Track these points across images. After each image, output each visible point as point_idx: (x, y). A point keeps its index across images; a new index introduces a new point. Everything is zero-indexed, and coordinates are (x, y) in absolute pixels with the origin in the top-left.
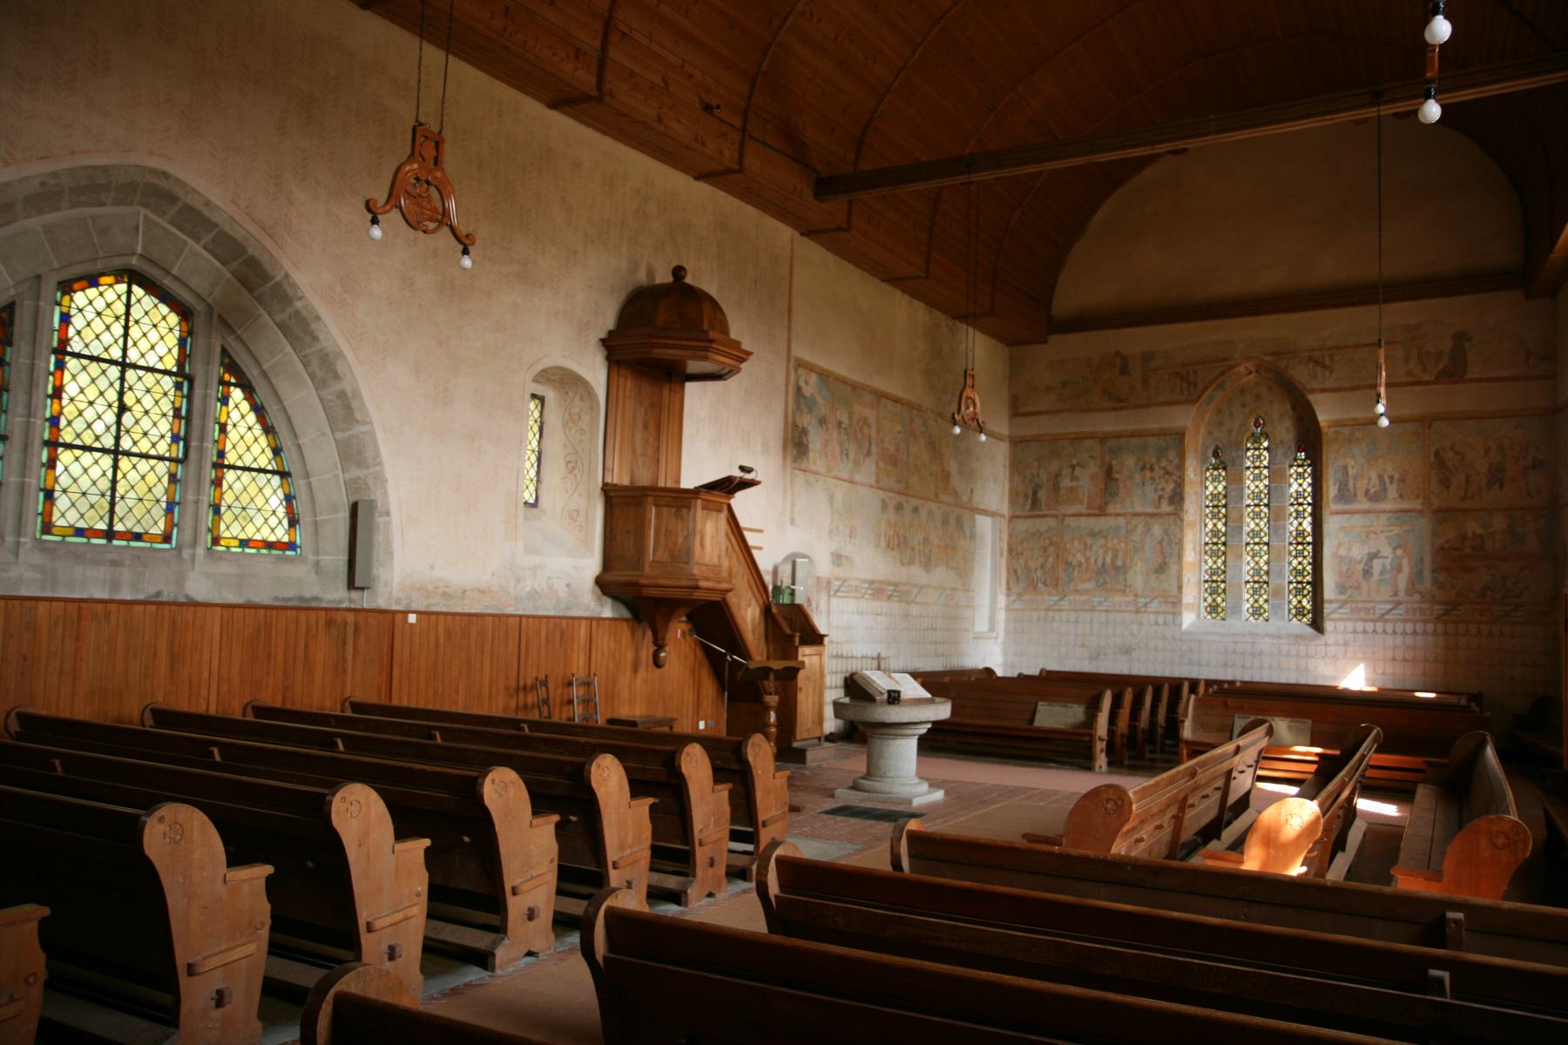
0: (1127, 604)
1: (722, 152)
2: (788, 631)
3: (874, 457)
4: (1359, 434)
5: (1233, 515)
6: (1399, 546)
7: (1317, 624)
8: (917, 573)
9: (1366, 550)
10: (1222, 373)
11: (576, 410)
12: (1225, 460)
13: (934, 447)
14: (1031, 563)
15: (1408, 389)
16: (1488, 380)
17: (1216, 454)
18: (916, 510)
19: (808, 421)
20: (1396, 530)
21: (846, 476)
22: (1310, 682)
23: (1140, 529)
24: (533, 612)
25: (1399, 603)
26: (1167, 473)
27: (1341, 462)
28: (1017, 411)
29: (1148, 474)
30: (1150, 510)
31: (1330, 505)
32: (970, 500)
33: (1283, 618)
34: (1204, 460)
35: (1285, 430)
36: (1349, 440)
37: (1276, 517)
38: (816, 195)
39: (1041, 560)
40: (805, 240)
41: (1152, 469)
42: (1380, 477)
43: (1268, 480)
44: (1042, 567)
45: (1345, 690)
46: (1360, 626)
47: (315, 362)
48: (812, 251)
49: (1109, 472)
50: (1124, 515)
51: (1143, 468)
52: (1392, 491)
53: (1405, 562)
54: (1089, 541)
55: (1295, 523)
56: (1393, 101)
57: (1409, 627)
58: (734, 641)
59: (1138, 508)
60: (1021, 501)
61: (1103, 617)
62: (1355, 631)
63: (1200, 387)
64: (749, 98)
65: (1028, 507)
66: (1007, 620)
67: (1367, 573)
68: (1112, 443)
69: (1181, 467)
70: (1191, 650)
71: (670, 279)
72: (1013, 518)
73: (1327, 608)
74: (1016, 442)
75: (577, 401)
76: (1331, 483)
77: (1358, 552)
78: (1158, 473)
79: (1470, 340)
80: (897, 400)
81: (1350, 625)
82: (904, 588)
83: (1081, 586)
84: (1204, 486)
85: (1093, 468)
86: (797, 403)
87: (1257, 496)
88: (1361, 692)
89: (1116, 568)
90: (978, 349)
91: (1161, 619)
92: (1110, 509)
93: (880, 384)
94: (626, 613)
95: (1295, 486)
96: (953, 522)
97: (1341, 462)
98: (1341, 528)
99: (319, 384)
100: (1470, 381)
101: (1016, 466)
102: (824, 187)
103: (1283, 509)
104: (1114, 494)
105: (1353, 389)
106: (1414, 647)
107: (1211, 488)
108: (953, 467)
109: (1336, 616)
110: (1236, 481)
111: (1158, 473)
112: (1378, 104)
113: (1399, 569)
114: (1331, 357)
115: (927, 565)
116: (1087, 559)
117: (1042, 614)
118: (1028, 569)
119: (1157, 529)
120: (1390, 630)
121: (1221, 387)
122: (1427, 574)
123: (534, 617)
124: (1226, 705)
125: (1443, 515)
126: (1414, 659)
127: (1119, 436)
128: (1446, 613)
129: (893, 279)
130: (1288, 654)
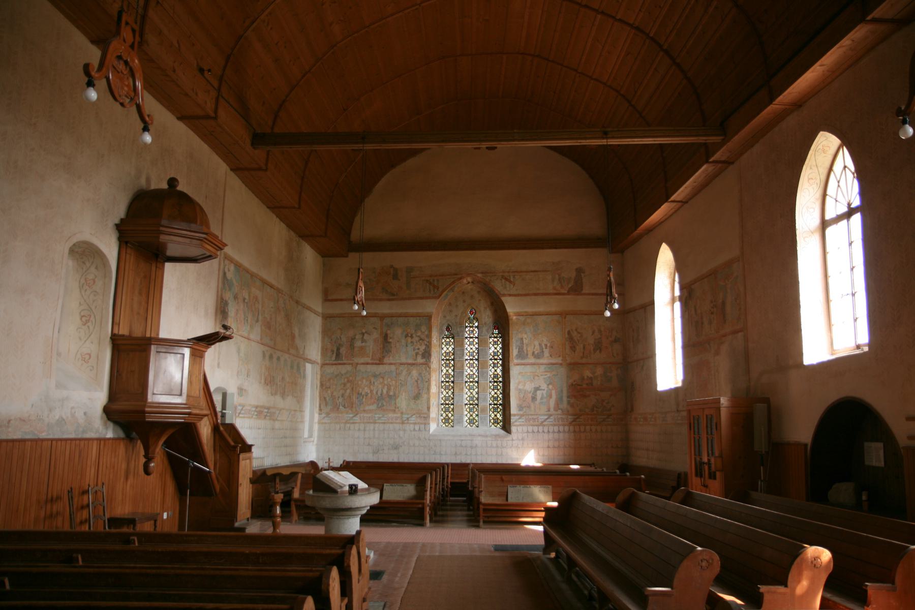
0: (397, 418)
1: (206, 102)
2: (232, 444)
4: (529, 321)
5: (458, 365)
6: (550, 384)
7: (506, 427)
8: (279, 401)
9: (533, 385)
10: (453, 282)
11: (91, 277)
12: (453, 332)
13: (288, 317)
16: (593, 294)
17: (448, 329)
18: (278, 359)
19: (228, 296)
20: (549, 374)
21: (246, 334)
22: (504, 462)
23: (404, 373)
24: (60, 437)
25: (551, 415)
28: (327, 297)
29: (409, 340)
30: (410, 361)
34: (441, 332)
35: (487, 316)
36: (524, 324)
37: (482, 366)
38: (252, 144)
39: (342, 392)
40: (232, 174)
41: (412, 337)
42: (540, 345)
43: (476, 344)
48: (235, 181)
49: (385, 337)
51: (407, 336)
52: (547, 353)
53: (553, 392)
56: (613, 138)
57: (556, 429)
58: (198, 454)
59: (404, 360)
61: (382, 427)
62: (528, 432)
63: (440, 290)
64: (224, 70)
65: (334, 358)
66: (319, 430)
67: (534, 398)
68: (387, 320)
69: (429, 336)
70: (435, 446)
71: (165, 186)
73: (513, 419)
74: (326, 317)
75: (93, 269)
77: (529, 387)
78: (416, 339)
80: (272, 286)
81: (525, 428)
82: (272, 410)
83: (367, 408)
85: (376, 335)
86: (224, 284)
87: (472, 354)
88: (534, 467)
89: (390, 397)
90: (309, 256)
91: (417, 428)
92: (386, 360)
93: (264, 275)
94: (121, 434)
96: (295, 367)
97: (520, 336)
98: (520, 373)
100: (585, 294)
103: (487, 362)
107: (445, 349)
108: (296, 331)
111: (416, 339)
112: (607, 138)
113: (551, 396)
114: (514, 277)
115: (283, 395)
116: (371, 391)
117: (342, 425)
119: (415, 373)
120: (546, 430)
121: (452, 290)
122: (565, 399)
123: (61, 440)
124: (502, 480)
125: (573, 366)
126: (559, 447)
127: (391, 316)
129: (275, 207)
130: (492, 446)
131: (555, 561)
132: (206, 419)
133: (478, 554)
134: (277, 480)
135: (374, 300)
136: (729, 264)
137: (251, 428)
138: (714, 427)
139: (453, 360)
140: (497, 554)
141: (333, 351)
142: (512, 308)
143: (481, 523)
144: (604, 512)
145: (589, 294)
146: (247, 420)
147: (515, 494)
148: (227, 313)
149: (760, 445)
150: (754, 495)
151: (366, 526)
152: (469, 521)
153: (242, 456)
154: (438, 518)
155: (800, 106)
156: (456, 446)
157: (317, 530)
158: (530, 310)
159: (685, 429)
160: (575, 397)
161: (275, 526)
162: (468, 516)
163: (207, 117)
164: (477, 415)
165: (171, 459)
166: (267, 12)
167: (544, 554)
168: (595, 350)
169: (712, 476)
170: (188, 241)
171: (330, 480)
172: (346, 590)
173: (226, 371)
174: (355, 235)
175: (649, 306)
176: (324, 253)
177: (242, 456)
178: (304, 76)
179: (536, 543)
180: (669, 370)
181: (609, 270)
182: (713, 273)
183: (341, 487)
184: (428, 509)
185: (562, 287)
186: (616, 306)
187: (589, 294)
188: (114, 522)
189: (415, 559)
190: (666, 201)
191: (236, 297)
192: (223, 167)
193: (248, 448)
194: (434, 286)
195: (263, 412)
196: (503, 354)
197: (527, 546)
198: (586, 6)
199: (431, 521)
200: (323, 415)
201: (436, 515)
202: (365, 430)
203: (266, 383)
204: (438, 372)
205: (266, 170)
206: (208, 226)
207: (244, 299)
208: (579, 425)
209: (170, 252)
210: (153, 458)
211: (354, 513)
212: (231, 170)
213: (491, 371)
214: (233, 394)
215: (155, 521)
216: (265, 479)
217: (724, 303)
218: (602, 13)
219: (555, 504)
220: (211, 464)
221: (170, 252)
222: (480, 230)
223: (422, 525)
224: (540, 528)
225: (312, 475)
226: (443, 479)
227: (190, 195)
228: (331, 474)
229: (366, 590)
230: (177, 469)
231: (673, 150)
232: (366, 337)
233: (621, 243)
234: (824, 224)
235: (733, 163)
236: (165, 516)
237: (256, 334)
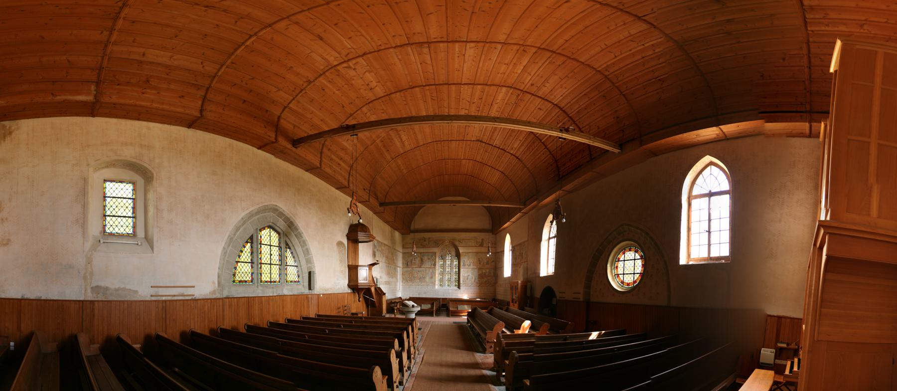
7: (459, 287)
12: (443, 258)
28: (404, 247)
35: (454, 253)
43: (450, 261)
48: (375, 217)
58: (371, 296)
74: (404, 253)
84: (439, 263)
90: (397, 235)
99: (302, 247)
101: (403, 258)
102: (381, 205)
125: (480, 269)
129: (387, 222)
142: (461, 250)
147: (460, 307)
149: (528, 294)
165: (365, 298)
172: (413, 331)
173: (377, 272)
174: (412, 228)
175: (503, 252)
176: (402, 234)
180: (507, 272)
182: (520, 244)
188: (353, 314)
195: (387, 283)
204: (438, 270)
222: (452, 225)
225: (401, 301)
230: (366, 300)
233: (495, 230)
234: (550, 238)
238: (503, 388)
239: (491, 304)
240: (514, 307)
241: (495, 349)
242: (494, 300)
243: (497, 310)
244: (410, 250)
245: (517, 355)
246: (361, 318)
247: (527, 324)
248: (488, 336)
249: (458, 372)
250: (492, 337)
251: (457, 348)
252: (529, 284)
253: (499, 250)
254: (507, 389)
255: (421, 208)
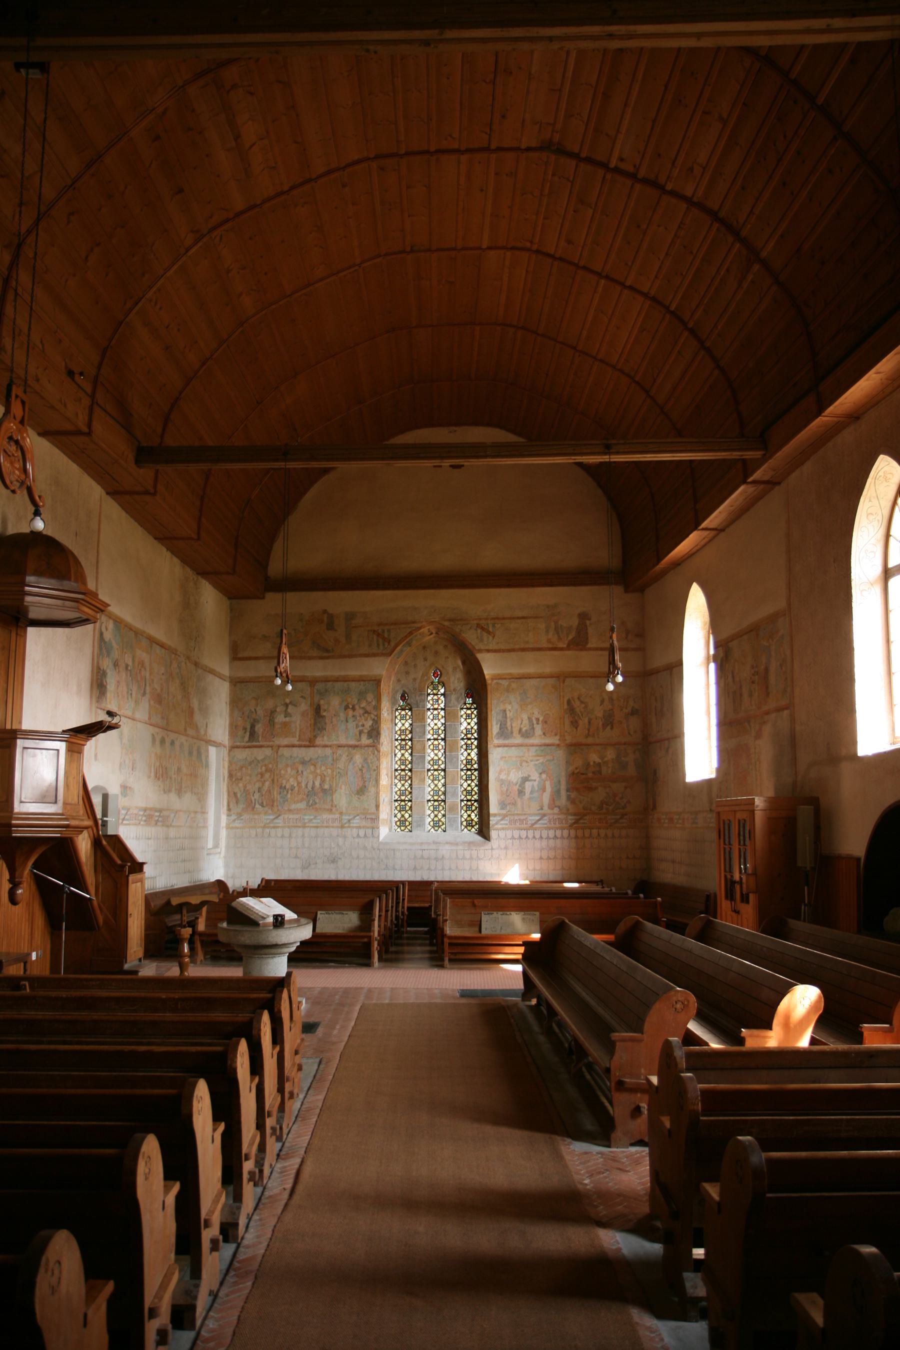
0: (334, 820)
1: (77, 414)
2: (119, 862)
3: (148, 696)
4: (514, 685)
5: (417, 746)
6: (544, 772)
7: (484, 831)
10: (410, 633)
12: (410, 701)
13: (184, 686)
14: (249, 787)
15: (548, 653)
17: (403, 698)
18: (172, 743)
19: (106, 664)
21: (130, 714)
22: (481, 879)
25: (544, 815)
26: (366, 712)
27: (502, 707)
28: (236, 655)
29: (350, 712)
31: (494, 740)
32: (206, 734)
33: (457, 829)
34: (394, 702)
35: (457, 681)
36: (508, 690)
37: (449, 748)
39: (258, 785)
40: (109, 499)
41: (354, 709)
42: (529, 718)
43: (442, 716)
44: (259, 790)
45: (507, 884)
46: (516, 833)
47: (284, 675)
48: (113, 509)
50: (330, 746)
51: (347, 708)
52: (538, 730)
53: (548, 784)
54: (300, 768)
55: (465, 754)
56: (618, 453)
57: (551, 833)
58: (74, 875)
59: (343, 741)
60: (240, 733)
61: (313, 832)
62: (513, 838)
63: (393, 644)
65: (247, 739)
66: (228, 837)
67: (521, 792)
68: (319, 686)
69: (378, 708)
70: (387, 857)
72: (233, 748)
73: (493, 821)
74: (236, 682)
76: (494, 723)
77: (515, 776)
79: (590, 619)
80: (162, 646)
81: (509, 833)
82: (165, 813)
83: (293, 806)
84: (393, 724)
85: (304, 706)
86: (100, 649)
88: (518, 886)
89: (324, 791)
90: (209, 598)
92: (319, 741)
93: (153, 631)
95: (465, 724)
96: (195, 753)
98: (502, 758)
100: (590, 649)
101: (235, 703)
103: (456, 742)
104: (323, 729)
105: (509, 651)
106: (555, 848)
107: (400, 725)
108: (195, 704)
109: (499, 826)
110: (419, 719)
112: (610, 454)
114: (494, 626)
115: (179, 792)
116: (299, 783)
118: (246, 791)
119: (358, 758)
120: (538, 836)
121: (409, 644)
122: (563, 793)
124: (474, 905)
125: (574, 748)
126: (555, 858)
127: (326, 680)
128: (577, 822)
129: (165, 537)
130: (464, 858)
131: (535, 1009)
132: (85, 834)
133: (438, 1001)
134: (185, 912)
135: (302, 658)
136: (773, 618)
137: (138, 838)
138: (747, 835)
139: (411, 740)
140: (463, 1001)
141: (245, 729)
142: (490, 667)
143: (446, 962)
144: (592, 947)
145: (596, 649)
146: (133, 828)
147: (492, 923)
148: (105, 687)
149: (805, 859)
150: (793, 923)
151: (295, 967)
152: (432, 959)
153: (132, 877)
154: (389, 956)
155: (858, 418)
156: (415, 857)
157: (235, 972)
158: (515, 671)
159: (714, 835)
160: (577, 790)
161: (182, 968)
162: (431, 952)
163: (79, 433)
164: (444, 816)
165: (41, 885)
166: (154, 289)
167: (523, 1000)
168: (604, 726)
169: (745, 899)
170: (59, 602)
171: (250, 909)
172: (277, 1038)
173: (106, 767)
174: (275, 568)
175: (676, 667)
176: (232, 594)
177: (132, 877)
178: (203, 364)
179: (515, 987)
180: (700, 757)
181: (612, 629)
182: (754, 630)
183: (264, 918)
184: (376, 944)
185: (560, 639)
186: (620, 679)
187: (596, 649)
189: (358, 1008)
190: (695, 528)
191: (116, 665)
192: (96, 491)
193: (138, 867)
194: (384, 639)
195: (154, 817)
196: (479, 731)
197: (503, 990)
198: (585, 268)
199: (380, 960)
200: (234, 817)
201: (387, 952)
202: (290, 837)
203: (157, 777)
205: (155, 494)
206: (84, 583)
207: (127, 666)
208: (583, 828)
209: (33, 614)
210: (20, 883)
211: (280, 950)
212: (108, 493)
213: (463, 756)
214: (117, 796)
215: (25, 963)
216: (167, 910)
217: (767, 670)
218: (607, 277)
219: (536, 936)
220: (92, 889)
221: (33, 614)
222: (446, 560)
223: (368, 964)
224: (519, 968)
225: (223, 901)
226: (398, 903)
227: (57, 539)
228: (250, 901)
229: (299, 1041)
230: (48, 897)
231: (693, 468)
232: (291, 709)
235: (779, 483)
236: (34, 956)
237: (142, 713)
238: (697, 1330)
239: (628, 903)
240: (740, 922)
241: (654, 1124)
242: (645, 886)
243: (657, 933)
244: (264, 669)
245: (759, 1157)
246: (14, 983)
247: (803, 998)
248: (621, 1055)
249: (487, 1238)
250: (637, 1060)
251: (500, 1119)
252: (805, 813)
253: (658, 662)
254: (716, 1338)
255: (314, 476)
